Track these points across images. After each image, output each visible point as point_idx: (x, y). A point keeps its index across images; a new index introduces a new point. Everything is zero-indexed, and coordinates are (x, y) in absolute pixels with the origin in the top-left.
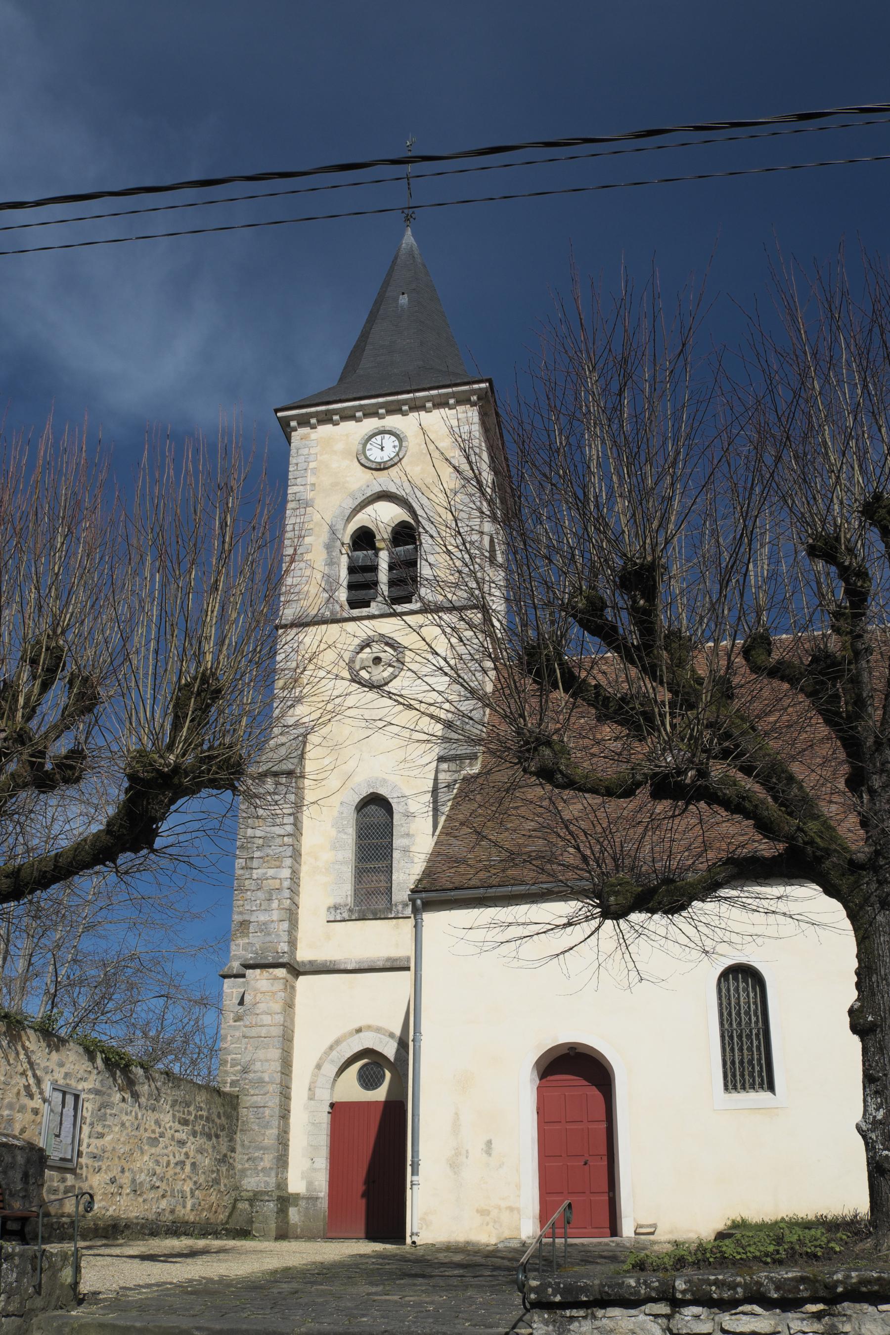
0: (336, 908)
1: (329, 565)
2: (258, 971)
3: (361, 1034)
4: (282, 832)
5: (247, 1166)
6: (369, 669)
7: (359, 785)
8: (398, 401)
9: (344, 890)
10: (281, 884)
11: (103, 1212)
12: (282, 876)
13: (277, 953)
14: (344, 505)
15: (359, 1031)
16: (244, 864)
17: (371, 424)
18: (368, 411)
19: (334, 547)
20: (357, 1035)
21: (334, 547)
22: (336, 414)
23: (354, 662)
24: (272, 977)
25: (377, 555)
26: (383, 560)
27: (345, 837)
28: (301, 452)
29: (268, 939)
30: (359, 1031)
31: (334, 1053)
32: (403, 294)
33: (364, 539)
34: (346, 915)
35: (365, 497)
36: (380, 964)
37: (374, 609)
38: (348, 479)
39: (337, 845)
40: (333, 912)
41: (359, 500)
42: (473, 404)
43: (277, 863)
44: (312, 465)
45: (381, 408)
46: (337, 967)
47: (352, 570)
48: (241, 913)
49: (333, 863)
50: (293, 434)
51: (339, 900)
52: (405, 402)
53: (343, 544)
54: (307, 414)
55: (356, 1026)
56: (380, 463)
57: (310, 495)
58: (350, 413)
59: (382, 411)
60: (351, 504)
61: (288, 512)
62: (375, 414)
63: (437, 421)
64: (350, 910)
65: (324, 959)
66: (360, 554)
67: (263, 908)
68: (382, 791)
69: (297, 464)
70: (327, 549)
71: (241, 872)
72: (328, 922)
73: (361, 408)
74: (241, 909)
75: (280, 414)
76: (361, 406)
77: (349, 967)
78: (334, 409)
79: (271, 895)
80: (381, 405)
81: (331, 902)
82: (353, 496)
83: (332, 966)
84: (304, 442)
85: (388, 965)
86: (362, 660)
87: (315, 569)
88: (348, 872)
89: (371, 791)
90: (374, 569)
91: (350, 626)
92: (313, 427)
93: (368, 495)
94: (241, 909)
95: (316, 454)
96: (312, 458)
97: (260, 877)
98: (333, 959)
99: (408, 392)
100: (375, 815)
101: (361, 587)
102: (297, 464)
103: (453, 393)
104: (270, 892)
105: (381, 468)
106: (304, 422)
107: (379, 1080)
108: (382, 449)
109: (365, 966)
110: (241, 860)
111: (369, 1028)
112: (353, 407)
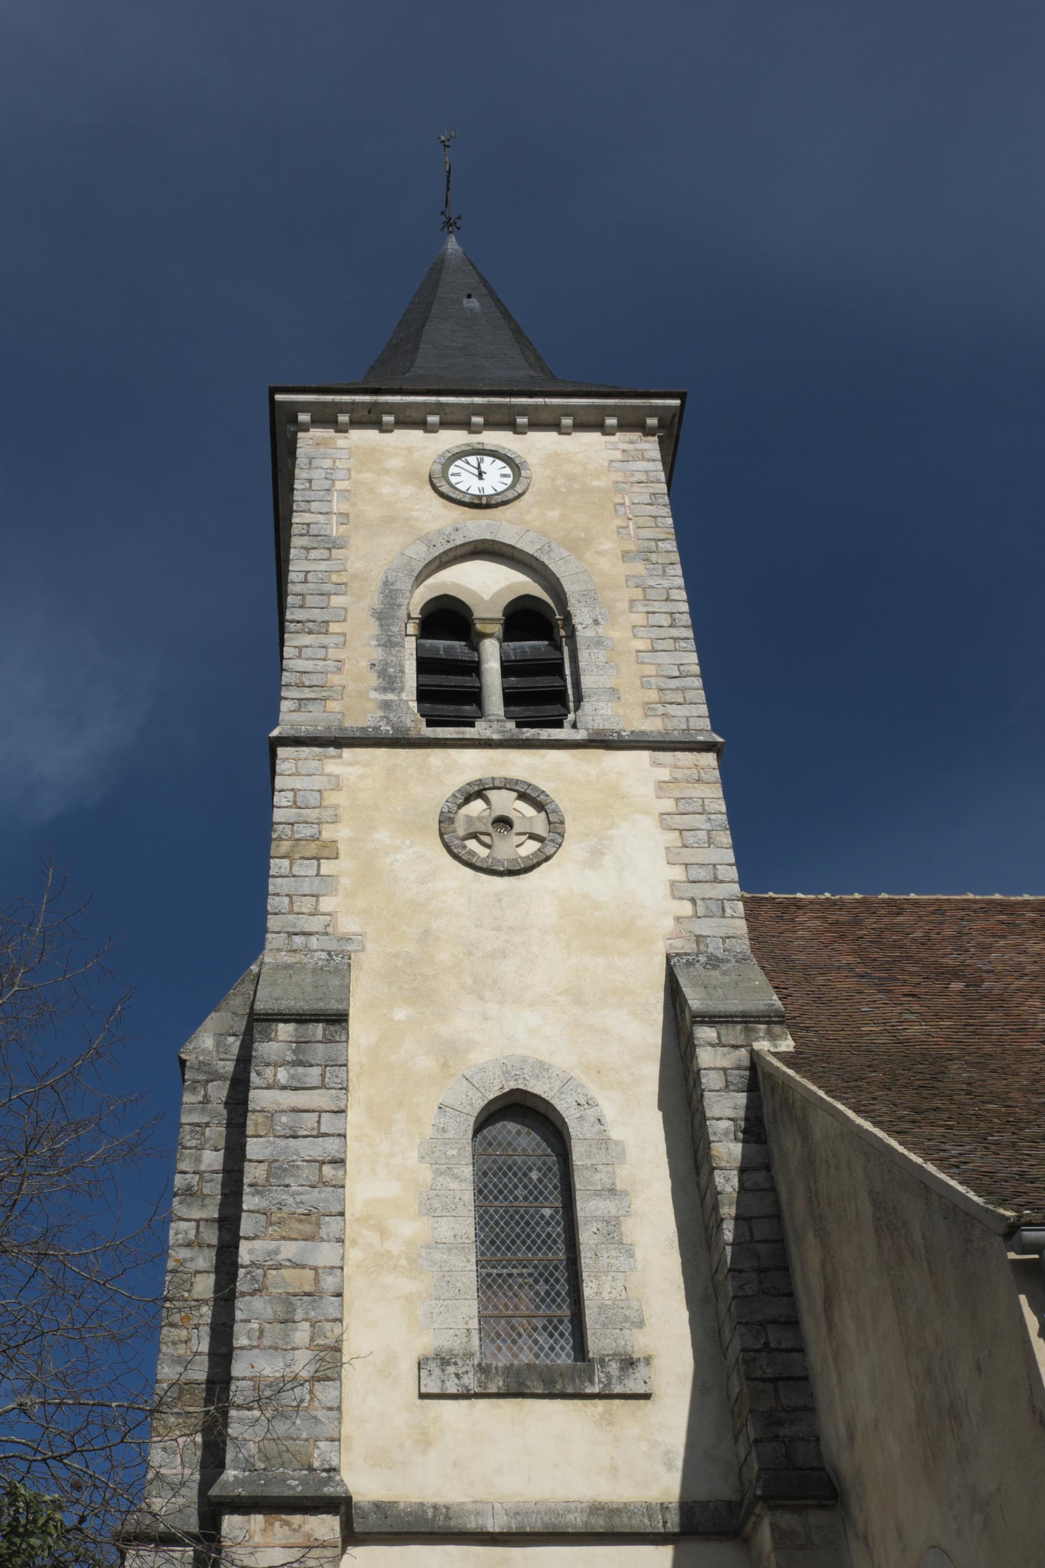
0: (444, 1360)
1: (385, 645)
2: (258, 1520)
4: (317, 1153)
6: (486, 839)
7: (483, 1070)
8: (511, 407)
9: (457, 1318)
10: (317, 1281)
12: (320, 1263)
13: (311, 1469)
14: (411, 552)
16: (192, 1234)
17: (454, 438)
18: (449, 418)
19: (393, 617)
21: (393, 617)
22: (389, 413)
23: (452, 821)
24: (298, 1539)
25: (475, 648)
26: (491, 656)
27: (454, 1185)
28: (315, 463)
29: (281, 1428)
32: (469, 296)
33: (447, 618)
34: (471, 1381)
35: (451, 545)
36: (576, 1521)
37: (480, 730)
38: (414, 514)
39: (436, 1203)
40: (437, 1371)
41: (440, 550)
42: (648, 432)
43: (307, 1228)
44: (340, 485)
45: (477, 414)
46: (455, 1524)
47: (424, 665)
48: (178, 1360)
49: (428, 1247)
50: (300, 435)
51: (448, 1342)
52: (523, 410)
53: (409, 617)
54: (333, 403)
56: (480, 497)
57: (335, 530)
58: (416, 415)
59: (477, 420)
60: (421, 555)
61: (292, 551)
62: (466, 425)
63: (589, 448)
64: (483, 1370)
66: (428, 642)
67: (267, 1342)
68: (538, 1087)
69: (310, 481)
70: (379, 619)
71: (183, 1253)
72: (422, 1396)
73: (438, 409)
74: (181, 1350)
75: (279, 397)
76: (440, 405)
77: (493, 1525)
78: (387, 404)
79: (291, 1308)
80: (477, 410)
81: (425, 1343)
82: (427, 540)
83: (441, 1520)
84: (322, 450)
85: (600, 1524)
86: (469, 819)
87: (346, 653)
88: (465, 1270)
89: (512, 1085)
90: (474, 668)
91: (436, 757)
92: (341, 429)
93: (458, 542)
94: (181, 1350)
95: (349, 470)
96: (339, 474)
97: (259, 1258)
98: (440, 1500)
99: (531, 395)
100: (523, 1135)
101: (447, 696)
102: (310, 481)
103: (616, 407)
104: (288, 1300)
105: (480, 504)
106: (325, 418)
108: (480, 475)
109: (535, 1523)
110: (183, 1225)
112: (424, 404)
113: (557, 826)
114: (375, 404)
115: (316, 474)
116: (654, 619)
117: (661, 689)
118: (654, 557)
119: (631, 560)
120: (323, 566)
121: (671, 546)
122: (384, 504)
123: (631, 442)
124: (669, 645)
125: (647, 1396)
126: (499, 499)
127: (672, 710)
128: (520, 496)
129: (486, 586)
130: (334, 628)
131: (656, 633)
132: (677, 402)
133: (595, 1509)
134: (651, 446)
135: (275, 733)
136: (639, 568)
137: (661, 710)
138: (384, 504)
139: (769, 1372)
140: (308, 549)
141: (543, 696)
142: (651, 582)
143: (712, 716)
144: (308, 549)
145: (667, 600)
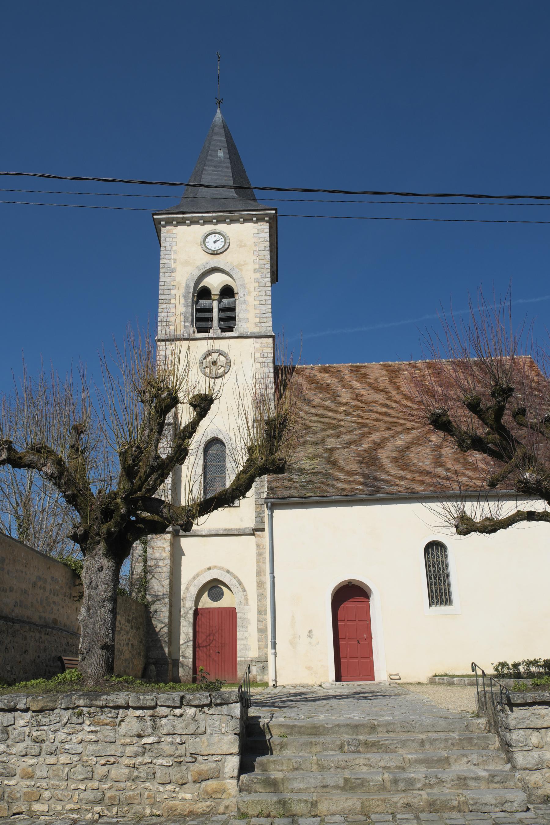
17: (209, 228)
33: (204, 293)
36: (221, 532)
37: (211, 334)
41: (202, 271)
44: (174, 248)
45: (214, 219)
56: (214, 251)
57: (173, 266)
63: (249, 226)
69: (165, 247)
70: (184, 297)
75: (155, 217)
80: (214, 218)
85: (225, 533)
89: (213, 436)
93: (207, 268)
101: (202, 321)
102: (165, 247)
106: (169, 222)
112: (198, 216)
113: (229, 364)
114: (183, 217)
115: (168, 244)
116: (261, 293)
117: (260, 318)
118: (263, 271)
119: (256, 272)
120: (169, 279)
121: (268, 266)
122: (187, 250)
123: (261, 226)
124: (264, 302)
125: (239, 507)
126: (219, 251)
127: (263, 324)
128: (226, 250)
129: (215, 282)
130: (172, 301)
131: (261, 298)
132: (274, 212)
133: (225, 530)
134: (265, 227)
135: (156, 338)
136: (258, 275)
137: (259, 325)
138: (187, 250)
139: (260, 503)
140: (165, 273)
141: (228, 321)
142: (261, 280)
143: (273, 326)
144: (165, 273)
145: (265, 286)
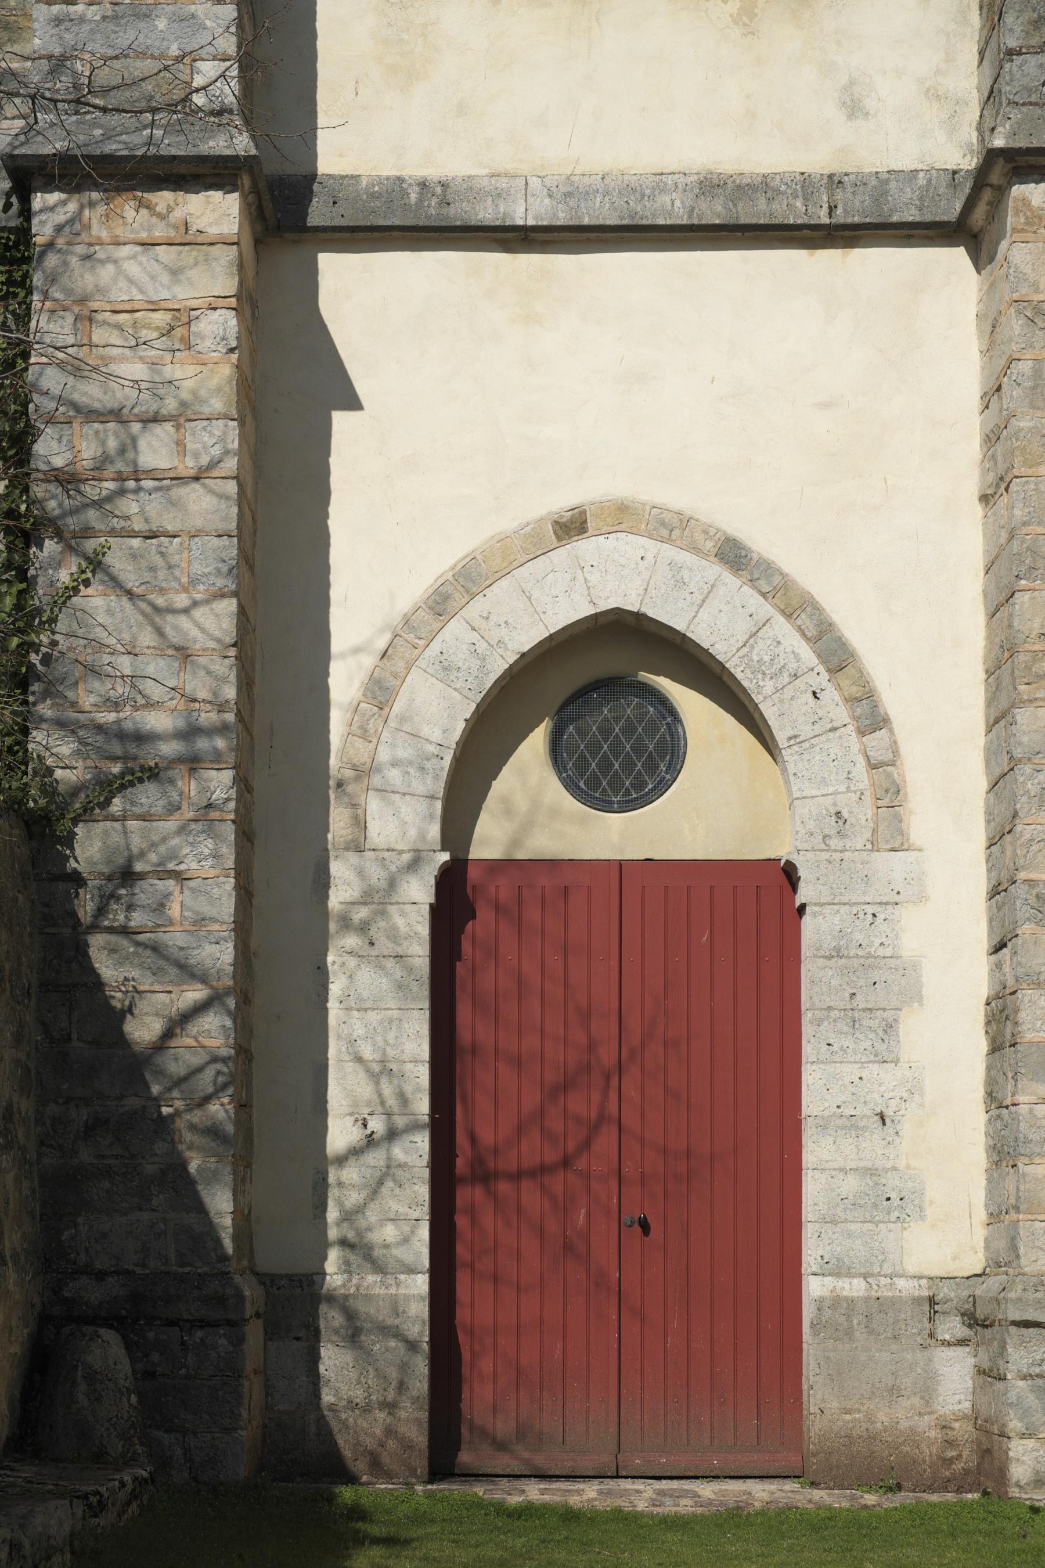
3: (584, 547)
5: (86, 1156)
11: (685, 1539)
15: (572, 526)
20: (561, 555)
30: (572, 526)
31: (455, 633)
36: (673, 209)
46: (465, 212)
55: (561, 501)
65: (388, 170)
77: (520, 215)
85: (714, 212)
107: (651, 767)
111: (623, 516)
